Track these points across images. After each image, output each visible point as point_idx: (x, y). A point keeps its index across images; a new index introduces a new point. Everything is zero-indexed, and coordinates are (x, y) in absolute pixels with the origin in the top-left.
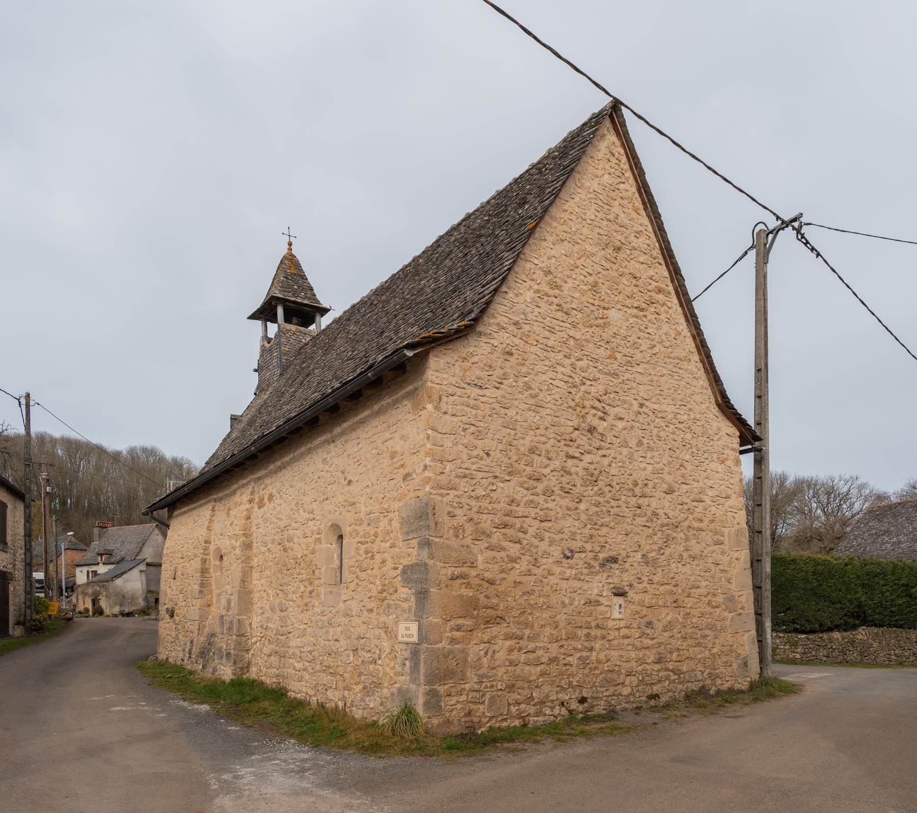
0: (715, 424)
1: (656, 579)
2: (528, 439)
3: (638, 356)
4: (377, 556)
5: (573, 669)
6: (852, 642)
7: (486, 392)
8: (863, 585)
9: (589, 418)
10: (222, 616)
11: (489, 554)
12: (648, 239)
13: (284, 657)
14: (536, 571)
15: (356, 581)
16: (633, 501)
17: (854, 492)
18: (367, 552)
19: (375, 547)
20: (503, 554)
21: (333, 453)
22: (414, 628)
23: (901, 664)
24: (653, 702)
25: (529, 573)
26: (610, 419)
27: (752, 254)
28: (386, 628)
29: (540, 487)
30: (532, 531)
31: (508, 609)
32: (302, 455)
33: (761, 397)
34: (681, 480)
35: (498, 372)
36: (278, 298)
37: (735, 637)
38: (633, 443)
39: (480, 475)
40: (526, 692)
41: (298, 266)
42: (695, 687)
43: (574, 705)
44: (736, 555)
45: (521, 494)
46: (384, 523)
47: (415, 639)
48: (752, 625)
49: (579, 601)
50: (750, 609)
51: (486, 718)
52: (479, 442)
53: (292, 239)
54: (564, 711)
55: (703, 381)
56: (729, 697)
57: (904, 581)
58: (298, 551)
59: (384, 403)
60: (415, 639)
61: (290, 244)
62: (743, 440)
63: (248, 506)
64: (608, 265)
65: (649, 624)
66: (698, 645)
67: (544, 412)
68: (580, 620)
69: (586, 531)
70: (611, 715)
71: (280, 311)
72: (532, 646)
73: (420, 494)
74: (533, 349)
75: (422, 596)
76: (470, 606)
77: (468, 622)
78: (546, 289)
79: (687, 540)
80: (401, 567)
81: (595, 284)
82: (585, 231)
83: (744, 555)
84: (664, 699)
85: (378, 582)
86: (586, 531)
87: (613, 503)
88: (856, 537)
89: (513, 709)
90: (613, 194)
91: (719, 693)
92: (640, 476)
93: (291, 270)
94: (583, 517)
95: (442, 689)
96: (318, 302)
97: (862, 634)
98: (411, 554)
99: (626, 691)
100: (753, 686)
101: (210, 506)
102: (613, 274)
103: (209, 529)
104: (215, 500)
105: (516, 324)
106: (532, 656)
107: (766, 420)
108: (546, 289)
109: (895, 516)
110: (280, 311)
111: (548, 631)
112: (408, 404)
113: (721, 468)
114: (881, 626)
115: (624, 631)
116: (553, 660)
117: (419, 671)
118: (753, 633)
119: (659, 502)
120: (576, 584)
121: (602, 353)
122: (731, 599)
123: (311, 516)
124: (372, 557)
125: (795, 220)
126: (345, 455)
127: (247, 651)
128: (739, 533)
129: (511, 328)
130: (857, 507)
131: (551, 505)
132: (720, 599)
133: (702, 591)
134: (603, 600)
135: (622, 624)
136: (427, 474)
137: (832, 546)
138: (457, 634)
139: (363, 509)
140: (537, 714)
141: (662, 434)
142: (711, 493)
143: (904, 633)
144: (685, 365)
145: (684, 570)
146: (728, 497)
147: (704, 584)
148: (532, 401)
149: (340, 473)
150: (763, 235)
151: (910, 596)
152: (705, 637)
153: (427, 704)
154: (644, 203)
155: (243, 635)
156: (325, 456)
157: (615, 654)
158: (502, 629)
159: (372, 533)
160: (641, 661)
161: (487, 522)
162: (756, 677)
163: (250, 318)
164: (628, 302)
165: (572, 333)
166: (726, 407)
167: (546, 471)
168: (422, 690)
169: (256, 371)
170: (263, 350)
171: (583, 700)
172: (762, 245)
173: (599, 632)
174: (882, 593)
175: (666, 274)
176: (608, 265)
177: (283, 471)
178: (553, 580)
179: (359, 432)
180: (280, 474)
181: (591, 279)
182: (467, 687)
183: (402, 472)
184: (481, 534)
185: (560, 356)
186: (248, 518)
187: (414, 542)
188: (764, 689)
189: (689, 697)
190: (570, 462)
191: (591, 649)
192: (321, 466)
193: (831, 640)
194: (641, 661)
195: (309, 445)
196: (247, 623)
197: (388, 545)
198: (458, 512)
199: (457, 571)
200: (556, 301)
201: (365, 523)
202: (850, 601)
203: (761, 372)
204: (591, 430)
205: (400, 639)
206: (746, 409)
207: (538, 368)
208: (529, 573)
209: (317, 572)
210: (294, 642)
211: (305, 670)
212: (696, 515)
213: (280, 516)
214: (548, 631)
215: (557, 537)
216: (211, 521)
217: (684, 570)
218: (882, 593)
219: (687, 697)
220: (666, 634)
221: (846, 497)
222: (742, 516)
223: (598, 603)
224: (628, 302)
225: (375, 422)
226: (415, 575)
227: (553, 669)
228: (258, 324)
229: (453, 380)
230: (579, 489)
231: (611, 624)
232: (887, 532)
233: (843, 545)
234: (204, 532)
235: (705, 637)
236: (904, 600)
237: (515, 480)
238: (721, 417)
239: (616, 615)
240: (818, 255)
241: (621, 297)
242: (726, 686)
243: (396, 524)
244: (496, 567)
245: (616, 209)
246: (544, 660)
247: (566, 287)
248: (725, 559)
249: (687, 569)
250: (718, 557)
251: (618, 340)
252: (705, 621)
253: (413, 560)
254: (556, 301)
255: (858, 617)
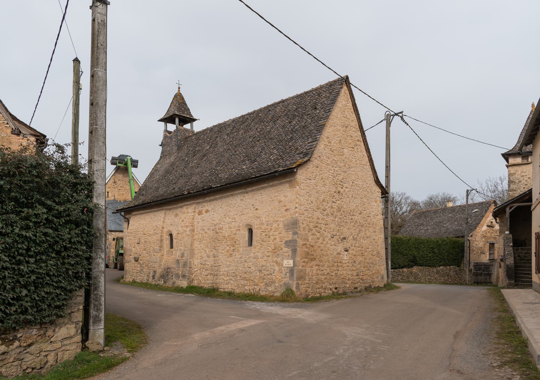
0: (374, 188)
1: (357, 245)
2: (322, 196)
3: (352, 165)
4: (272, 237)
5: (333, 277)
6: (411, 273)
7: (312, 181)
8: (415, 248)
9: (338, 188)
10: (178, 260)
11: (312, 236)
12: (355, 123)
13: (217, 275)
14: (324, 242)
15: (260, 246)
16: (350, 217)
17: (403, 201)
18: (266, 235)
19: (271, 234)
20: (315, 237)
21: (247, 197)
22: (291, 262)
23: (430, 283)
24: (356, 290)
25: (322, 243)
26: (344, 188)
27: (385, 122)
28: (277, 263)
29: (325, 213)
30: (323, 228)
31: (317, 255)
32: (228, 196)
33: (388, 177)
34: (364, 209)
35: (315, 174)
36: (177, 115)
37: (379, 268)
38: (350, 196)
39: (310, 209)
40: (321, 285)
41: (183, 99)
42: (367, 285)
43: (334, 290)
44: (380, 236)
45: (321, 216)
46: (275, 225)
47: (292, 265)
48: (385, 263)
49: (335, 253)
50: (384, 257)
51: (311, 294)
52: (310, 199)
53: (180, 86)
54: (331, 292)
55: (371, 172)
56: (378, 289)
57: (432, 246)
58: (226, 233)
59: (275, 183)
60: (292, 265)
61: (179, 88)
62: (382, 194)
63: (193, 214)
64: (344, 133)
65: (355, 261)
66: (368, 270)
67: (326, 187)
68: (335, 260)
69: (337, 228)
70: (345, 293)
71: (177, 120)
72: (323, 268)
73: (293, 216)
74: (324, 165)
75: (294, 251)
76: (307, 254)
77: (306, 260)
78: (327, 143)
79: (366, 231)
80: (284, 241)
81: (340, 141)
82: (338, 122)
83: (382, 236)
84: (359, 289)
85: (272, 246)
86: (337, 228)
87: (345, 218)
88: (409, 226)
89: (318, 290)
90: (345, 108)
91: (375, 288)
92: (352, 208)
93: (179, 100)
94: (337, 223)
95: (300, 282)
96: (192, 116)
97: (415, 269)
98: (289, 236)
99: (348, 286)
100: (385, 286)
101: (163, 212)
102: (345, 136)
103: (164, 222)
104: (166, 209)
105: (319, 157)
106: (322, 272)
107: (390, 186)
108: (327, 143)
109: (425, 217)
110: (177, 120)
111: (327, 263)
112: (287, 185)
113: (375, 204)
114: (422, 266)
115: (347, 264)
116: (328, 274)
117: (293, 276)
118: (385, 266)
119: (357, 217)
120: (334, 247)
121: (342, 164)
122: (378, 253)
123: (234, 220)
124: (269, 237)
125: (400, 113)
126: (254, 199)
127: (192, 274)
128: (381, 228)
129: (318, 158)
130: (404, 209)
131: (328, 219)
132: (375, 253)
133: (370, 250)
134: (342, 253)
135: (347, 261)
136: (297, 210)
137: (397, 230)
138: (304, 264)
139: (264, 219)
140: (325, 292)
141: (359, 192)
142: (373, 214)
143: (431, 269)
144: (365, 167)
145: (364, 242)
146: (378, 215)
147: (370, 247)
148: (323, 183)
149: (251, 205)
150: (389, 116)
151: (434, 253)
152: (370, 267)
153: (296, 287)
154: (354, 110)
155: (191, 268)
156: (242, 198)
157: (345, 272)
158: (313, 263)
159: (269, 228)
160: (352, 275)
161: (311, 225)
162: (386, 282)
163: (159, 121)
164: (349, 146)
165: (334, 158)
166: (377, 182)
167: (327, 207)
168: (295, 282)
169: (160, 145)
170: (165, 137)
171: (336, 288)
172: (388, 119)
173: (340, 264)
174: (423, 251)
175: (360, 134)
176: (344, 133)
177: (215, 201)
178: (328, 245)
179: (262, 191)
180: (213, 202)
181: (339, 139)
182: (306, 282)
183: (285, 208)
184: (310, 230)
185: (331, 167)
186: (193, 219)
187: (291, 233)
188: (388, 287)
189: (366, 289)
190: (333, 204)
191: (338, 270)
192: (239, 202)
193: (403, 272)
194: (352, 275)
195: (232, 193)
196: (192, 262)
197: (277, 233)
198: (304, 222)
199: (304, 243)
200: (330, 147)
201: (265, 225)
202: (411, 255)
203: (388, 168)
204: (339, 192)
205: (284, 266)
206: (383, 182)
207: (325, 172)
208: (322, 243)
209: (237, 242)
210: (223, 269)
211: (231, 280)
212: (368, 222)
213: (213, 219)
214: (327, 263)
215: (330, 231)
216: (164, 219)
217: (364, 242)
218: (423, 251)
219: (366, 289)
220: (359, 265)
221: (399, 203)
222: (382, 222)
223: (340, 254)
224: (349, 146)
225: (271, 189)
226: (291, 244)
227: (328, 277)
228: (163, 123)
229: (304, 178)
230: (335, 213)
231: (344, 261)
232: (422, 224)
233: (403, 230)
234: (161, 223)
235: (370, 267)
236: (432, 254)
237: (319, 211)
238: (376, 185)
239: (345, 258)
240: (407, 124)
241: (347, 144)
242: (377, 285)
243: (281, 226)
244: (314, 241)
245: (346, 113)
246: (326, 274)
247: (332, 142)
248: (377, 238)
249: (365, 242)
250: (374, 237)
251: (346, 160)
252: (371, 261)
253: (290, 238)
254: (330, 147)
255: (413, 262)
